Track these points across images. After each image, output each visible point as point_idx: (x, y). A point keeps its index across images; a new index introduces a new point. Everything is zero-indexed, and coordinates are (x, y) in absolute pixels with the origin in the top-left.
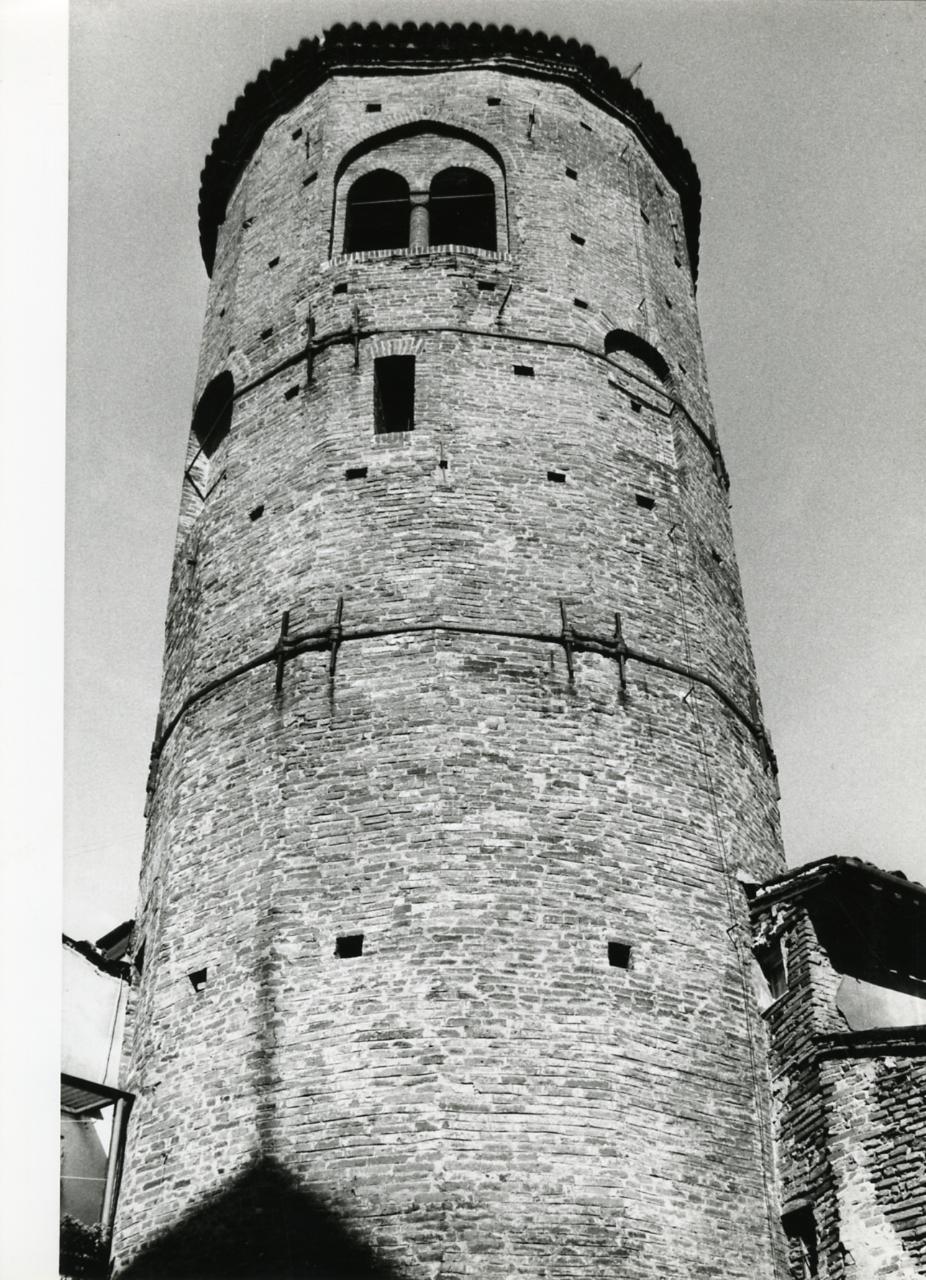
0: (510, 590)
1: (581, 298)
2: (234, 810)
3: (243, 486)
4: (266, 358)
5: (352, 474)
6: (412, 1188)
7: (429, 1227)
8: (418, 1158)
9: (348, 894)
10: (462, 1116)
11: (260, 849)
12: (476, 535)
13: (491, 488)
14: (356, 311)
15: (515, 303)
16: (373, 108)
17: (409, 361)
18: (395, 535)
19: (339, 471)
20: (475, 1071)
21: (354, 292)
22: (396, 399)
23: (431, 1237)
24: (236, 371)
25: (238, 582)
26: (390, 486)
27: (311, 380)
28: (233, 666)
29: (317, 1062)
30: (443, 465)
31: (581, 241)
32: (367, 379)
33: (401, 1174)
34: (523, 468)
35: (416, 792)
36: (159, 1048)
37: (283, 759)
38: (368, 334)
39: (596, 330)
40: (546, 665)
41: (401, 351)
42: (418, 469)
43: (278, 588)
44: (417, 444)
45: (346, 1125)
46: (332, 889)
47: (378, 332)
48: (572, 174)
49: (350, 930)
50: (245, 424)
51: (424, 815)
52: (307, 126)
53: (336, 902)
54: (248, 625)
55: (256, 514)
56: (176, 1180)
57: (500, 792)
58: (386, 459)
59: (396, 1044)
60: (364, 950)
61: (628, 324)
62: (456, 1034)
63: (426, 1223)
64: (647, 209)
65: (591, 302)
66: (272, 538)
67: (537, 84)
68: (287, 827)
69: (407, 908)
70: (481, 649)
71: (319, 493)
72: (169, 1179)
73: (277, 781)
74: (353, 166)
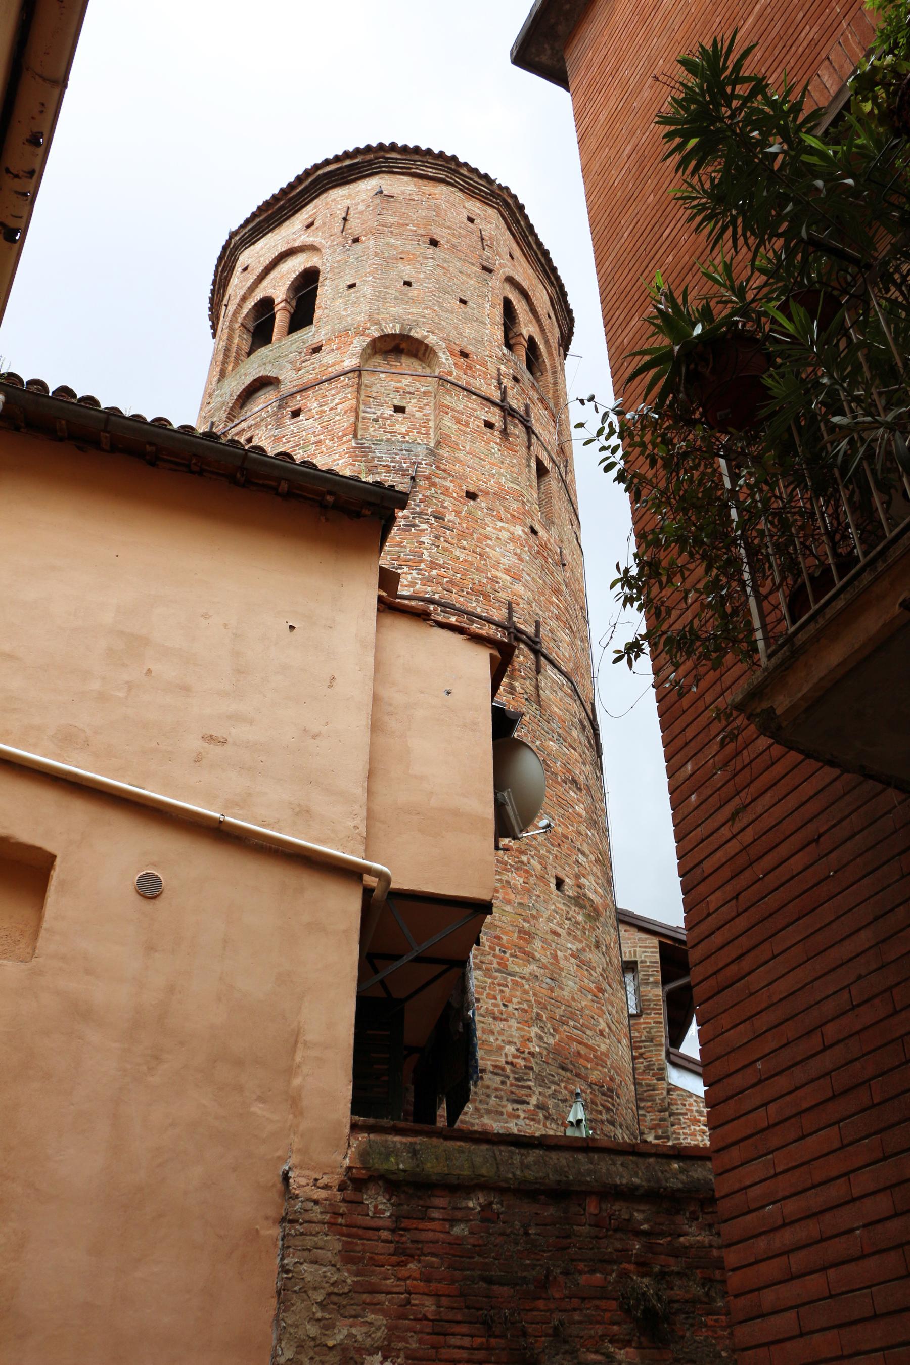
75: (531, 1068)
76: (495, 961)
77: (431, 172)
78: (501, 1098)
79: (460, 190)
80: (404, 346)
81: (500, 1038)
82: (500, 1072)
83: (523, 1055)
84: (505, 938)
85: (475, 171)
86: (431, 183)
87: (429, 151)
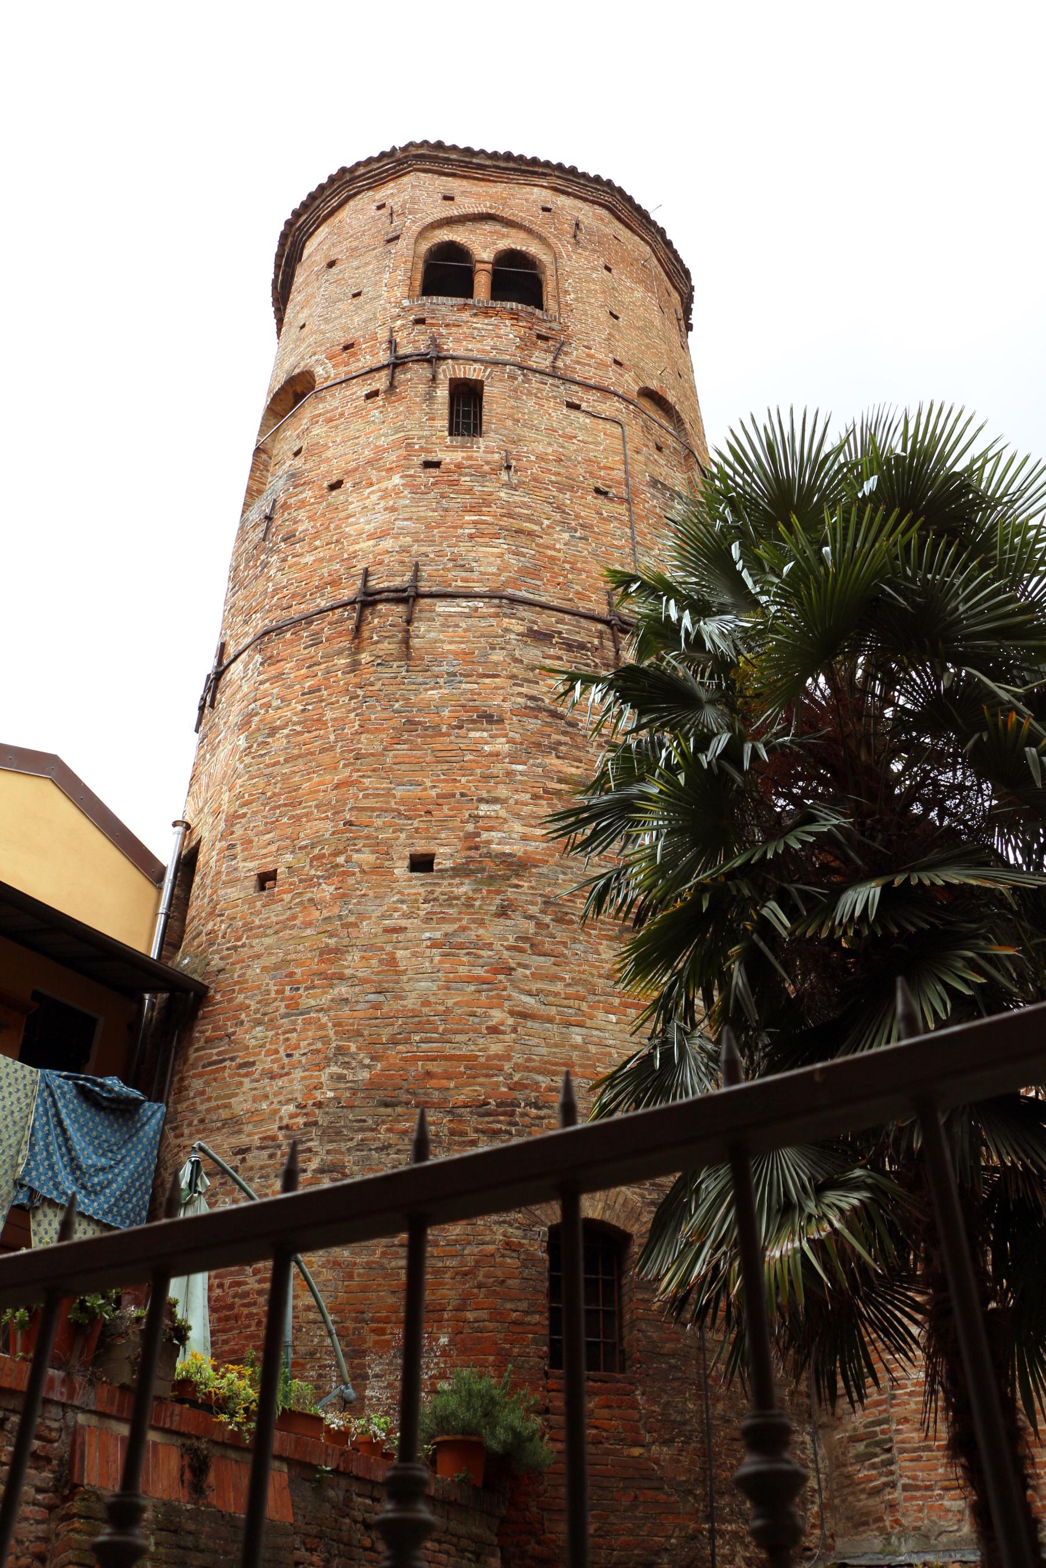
0: (565, 577)
1: (618, 358)
2: (309, 732)
3: (322, 462)
4: (347, 365)
5: (428, 465)
6: (481, 1085)
7: (499, 1122)
8: (489, 1058)
9: (421, 816)
10: (529, 1024)
11: (335, 768)
12: (536, 528)
13: (548, 493)
14: (433, 339)
15: (566, 354)
16: (448, 198)
17: (480, 384)
18: (467, 518)
19: (417, 460)
20: (540, 985)
21: (433, 325)
22: (466, 406)
23: (500, 1131)
24: (319, 371)
25: (315, 538)
26: (463, 479)
27: (392, 386)
28: (312, 608)
29: (392, 961)
30: (509, 467)
31: (617, 318)
32: (442, 393)
33: (472, 1072)
34: (574, 480)
35: (485, 734)
36: (223, 937)
37: (360, 692)
38: (445, 358)
39: (629, 384)
40: (596, 642)
41: (472, 376)
42: (486, 468)
43: (357, 547)
44: (485, 449)
45: (420, 1023)
46: (405, 810)
47: (453, 358)
48: (608, 269)
49: (421, 847)
50: (327, 412)
51: (491, 754)
52: (390, 202)
53: (410, 822)
54: (326, 575)
55: (336, 486)
56: (239, 1061)
57: (560, 743)
58: (459, 456)
59: (467, 954)
60: (435, 868)
61: (654, 385)
62: (522, 950)
63: (495, 1118)
64: (662, 304)
65: (625, 362)
66: (351, 507)
67: (579, 204)
68: (363, 751)
69: (478, 835)
70: (546, 621)
71: (399, 475)
72: (232, 1059)
73: (354, 710)
74: (429, 235)
75: (315, 1123)
76: (283, 1004)
77: (334, 203)
78: (266, 1177)
79: (368, 189)
80: (299, 389)
81: (275, 1101)
82: (270, 1143)
83: (305, 1111)
84: (298, 971)
85: (370, 160)
86: (340, 211)
87: (321, 188)
